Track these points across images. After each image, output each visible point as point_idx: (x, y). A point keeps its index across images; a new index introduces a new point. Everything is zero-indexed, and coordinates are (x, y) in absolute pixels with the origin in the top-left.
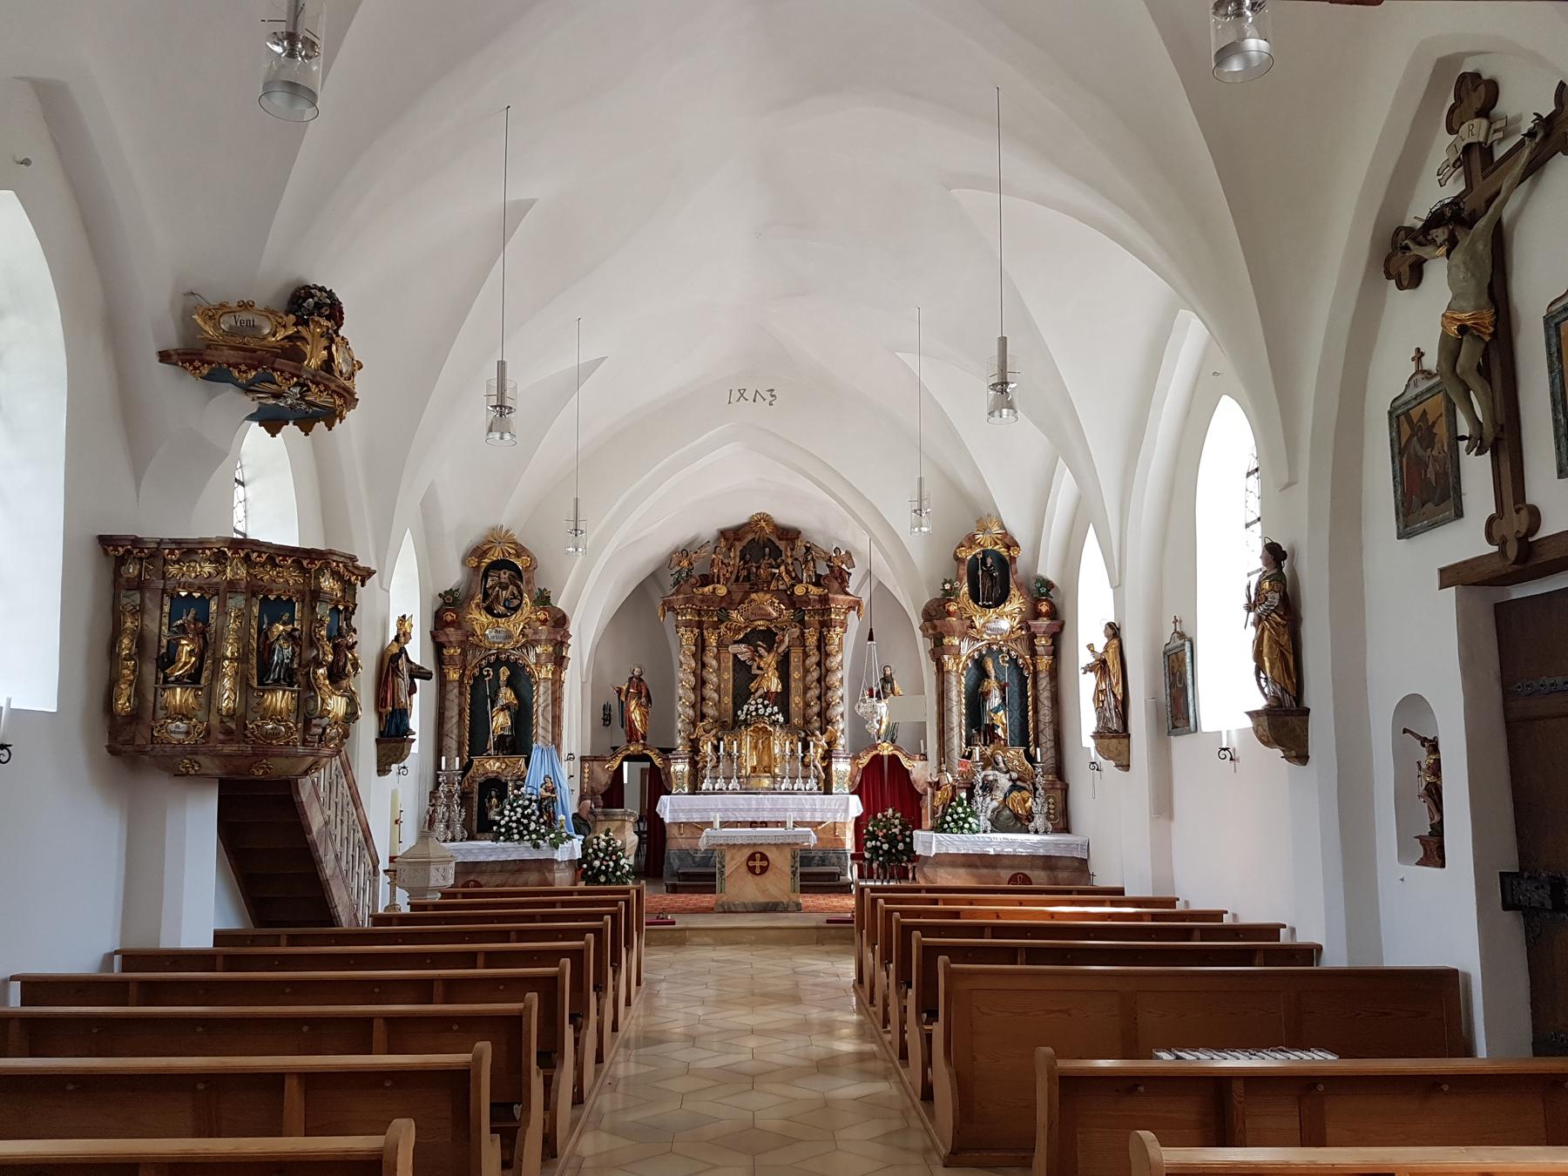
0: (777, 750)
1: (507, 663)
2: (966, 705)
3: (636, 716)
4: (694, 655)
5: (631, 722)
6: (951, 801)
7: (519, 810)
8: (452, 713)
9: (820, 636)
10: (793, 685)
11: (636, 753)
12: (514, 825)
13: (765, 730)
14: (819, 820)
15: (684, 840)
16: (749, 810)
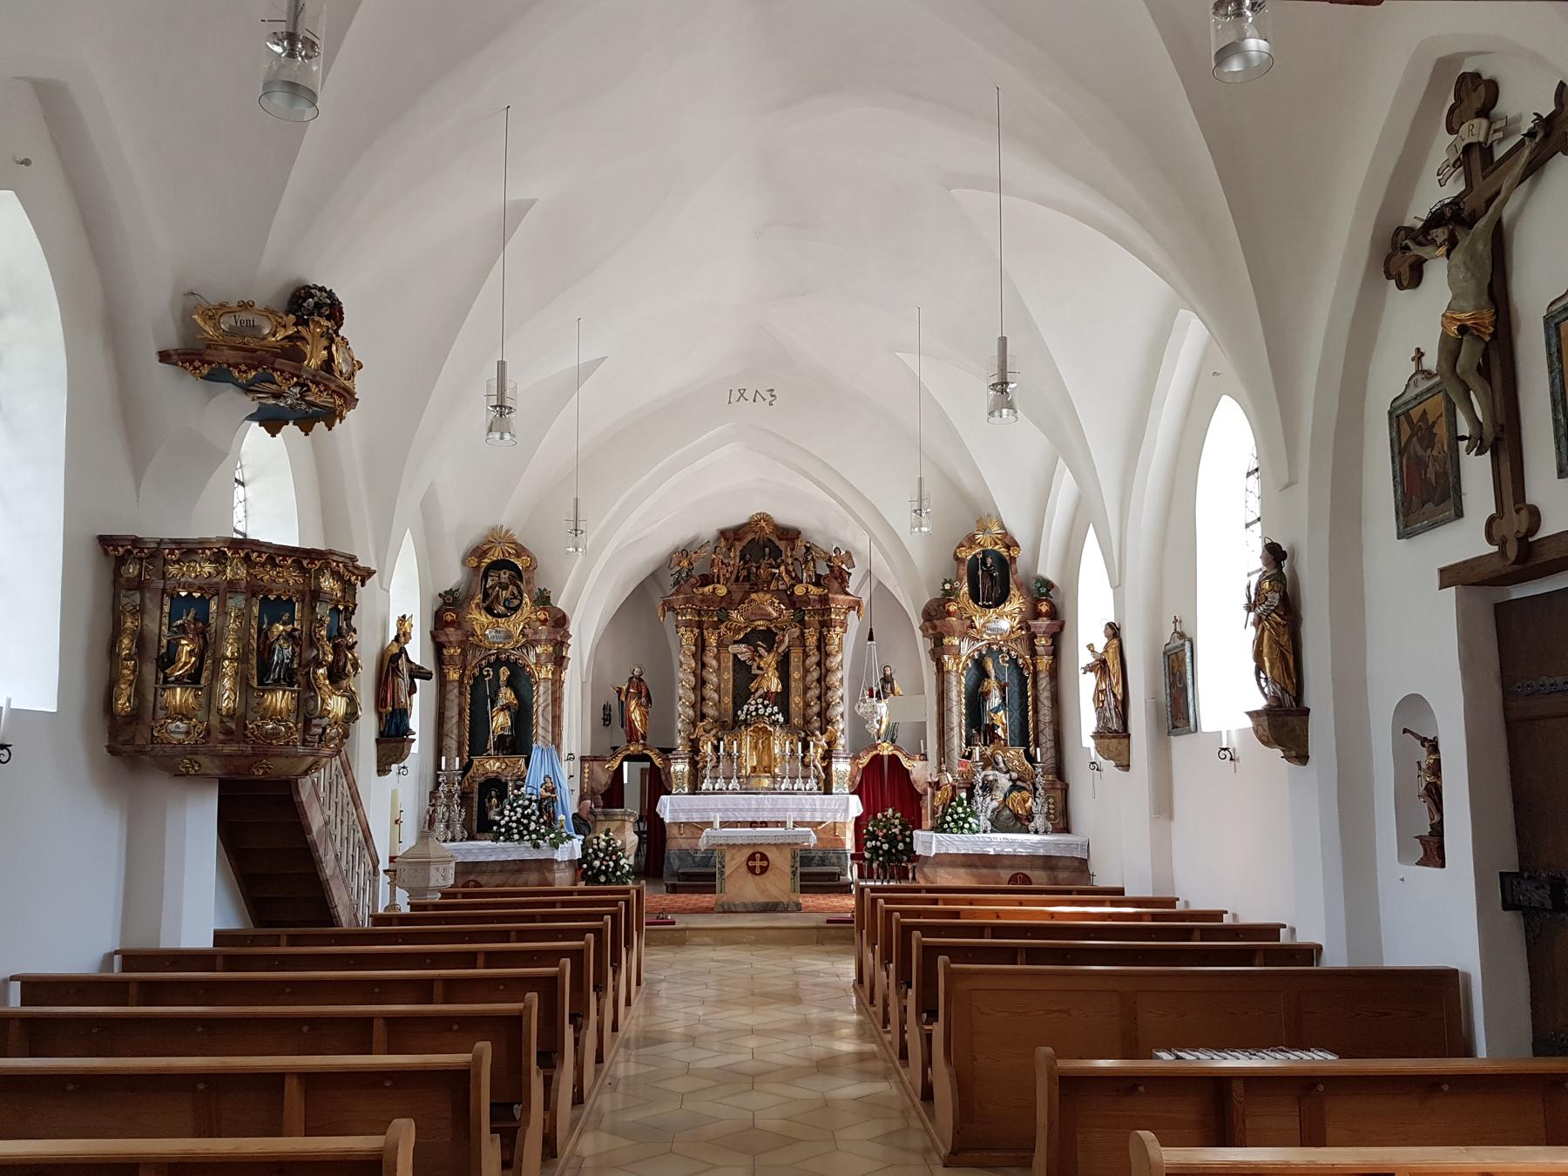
0: (777, 750)
1: (507, 663)
2: (966, 705)
3: (636, 716)
4: (694, 655)
5: (631, 722)
6: (951, 801)
7: (519, 810)
8: (452, 713)
9: (820, 636)
10: (793, 685)
11: (636, 753)
12: (514, 825)
13: (765, 730)
14: (819, 820)
15: (684, 840)
16: (749, 810)
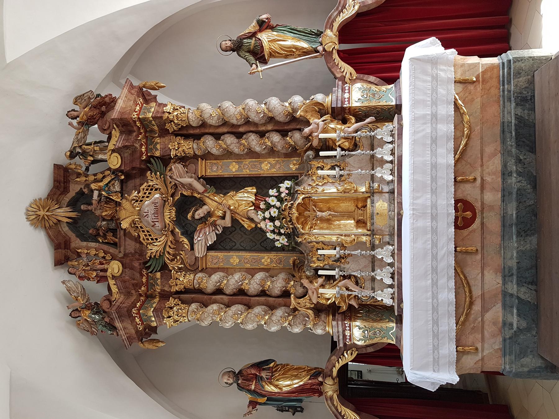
0: (332, 190)
4: (205, 305)
9: (181, 135)
10: (246, 172)
11: (336, 387)
13: (303, 207)
14: (452, 108)
15: (486, 345)
16: (434, 231)
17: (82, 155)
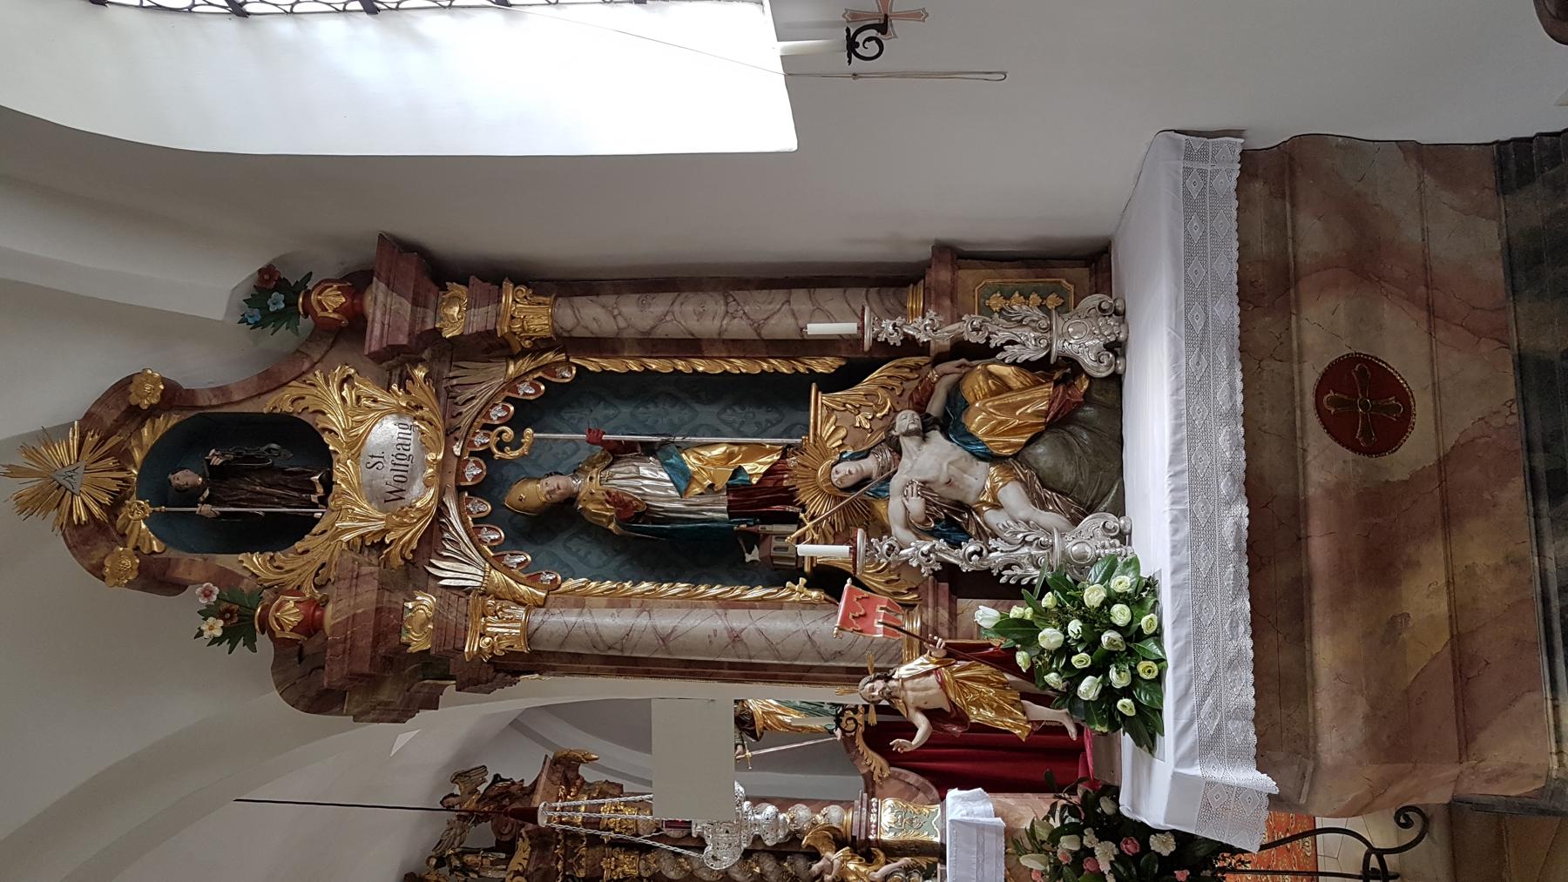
2: (696, 582)
6: (1015, 670)
17: (461, 871)
